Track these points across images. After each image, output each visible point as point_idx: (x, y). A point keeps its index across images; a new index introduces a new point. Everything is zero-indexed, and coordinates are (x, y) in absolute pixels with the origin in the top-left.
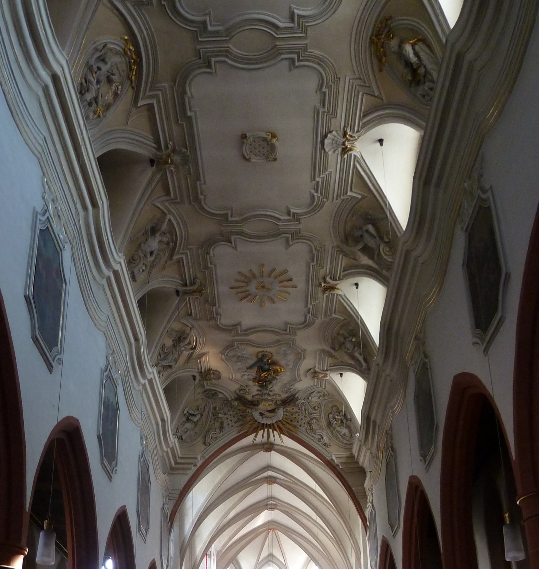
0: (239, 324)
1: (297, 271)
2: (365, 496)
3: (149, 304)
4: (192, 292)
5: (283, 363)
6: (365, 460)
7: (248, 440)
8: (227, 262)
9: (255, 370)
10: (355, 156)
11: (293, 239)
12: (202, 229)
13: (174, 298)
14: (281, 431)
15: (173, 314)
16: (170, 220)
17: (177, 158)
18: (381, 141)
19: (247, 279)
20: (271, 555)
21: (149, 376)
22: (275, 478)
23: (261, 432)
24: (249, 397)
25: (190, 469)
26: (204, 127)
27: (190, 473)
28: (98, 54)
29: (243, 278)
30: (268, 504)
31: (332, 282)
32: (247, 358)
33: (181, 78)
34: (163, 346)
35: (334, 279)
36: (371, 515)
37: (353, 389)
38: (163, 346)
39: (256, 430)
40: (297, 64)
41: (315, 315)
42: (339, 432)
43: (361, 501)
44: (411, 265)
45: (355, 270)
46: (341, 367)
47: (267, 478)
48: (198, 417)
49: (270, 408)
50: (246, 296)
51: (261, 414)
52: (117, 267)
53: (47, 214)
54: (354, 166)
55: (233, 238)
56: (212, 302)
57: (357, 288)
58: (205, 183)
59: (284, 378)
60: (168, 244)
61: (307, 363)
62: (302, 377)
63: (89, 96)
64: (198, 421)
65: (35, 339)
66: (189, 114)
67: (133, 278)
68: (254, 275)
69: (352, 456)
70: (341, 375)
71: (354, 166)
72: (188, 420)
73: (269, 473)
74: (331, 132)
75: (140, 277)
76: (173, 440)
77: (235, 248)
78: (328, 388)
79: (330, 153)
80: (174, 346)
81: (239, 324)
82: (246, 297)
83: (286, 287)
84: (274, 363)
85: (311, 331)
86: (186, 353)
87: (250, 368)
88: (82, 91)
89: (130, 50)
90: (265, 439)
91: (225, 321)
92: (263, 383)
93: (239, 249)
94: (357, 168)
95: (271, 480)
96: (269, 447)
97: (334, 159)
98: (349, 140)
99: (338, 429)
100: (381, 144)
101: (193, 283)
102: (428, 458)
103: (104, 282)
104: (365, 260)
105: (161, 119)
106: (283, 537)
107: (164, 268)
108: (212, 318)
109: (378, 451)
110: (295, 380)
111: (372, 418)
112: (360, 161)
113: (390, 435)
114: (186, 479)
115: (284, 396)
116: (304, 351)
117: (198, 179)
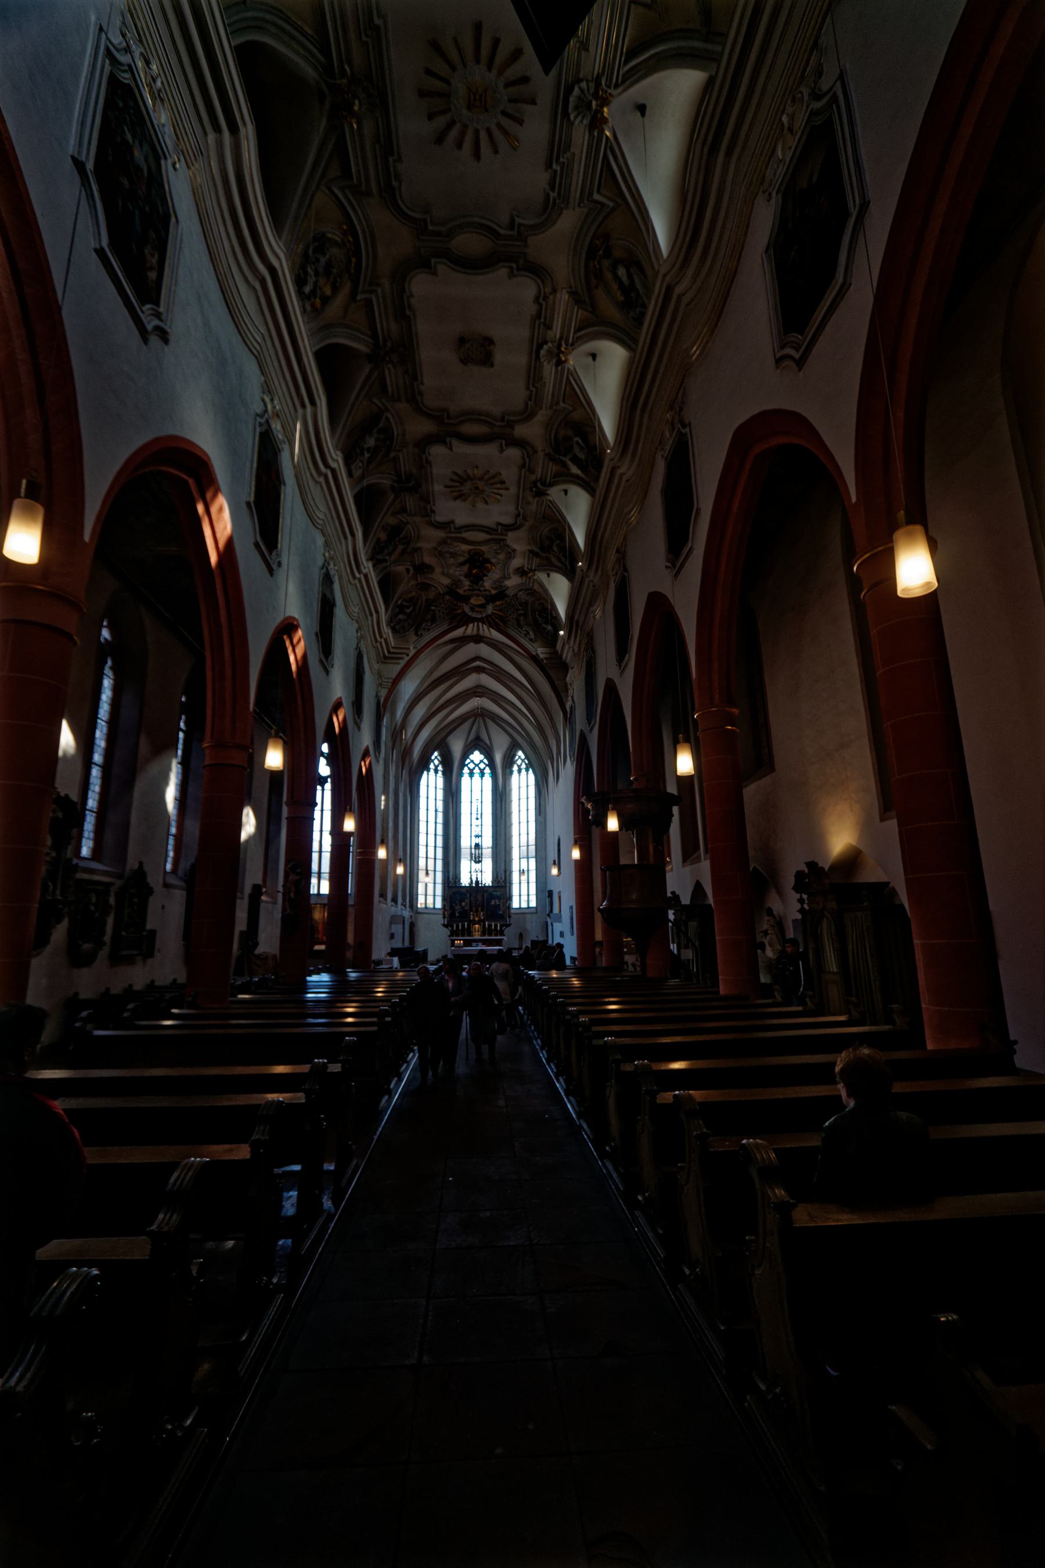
0: (453, 522)
1: (510, 474)
2: (567, 690)
3: (368, 502)
5: (493, 561)
6: (567, 655)
7: (459, 632)
8: (443, 460)
11: (507, 445)
12: (419, 427)
13: (386, 502)
14: (490, 626)
15: (388, 509)
16: (387, 418)
18: (594, 356)
19: (462, 479)
20: (478, 738)
21: (365, 571)
22: (484, 668)
23: (471, 625)
24: (461, 592)
25: (402, 658)
26: (423, 327)
27: (402, 663)
29: (455, 478)
30: (479, 691)
33: (401, 274)
34: (379, 539)
36: (571, 708)
37: (559, 591)
39: (466, 624)
41: (525, 519)
43: (563, 695)
44: (616, 481)
45: (564, 477)
46: (549, 567)
47: (475, 667)
49: (479, 603)
50: (460, 497)
51: (472, 609)
52: (334, 465)
53: (266, 416)
54: (568, 378)
56: (427, 499)
57: (643, 114)
58: (422, 383)
59: (495, 575)
61: (517, 562)
63: (307, 289)
65: (257, 545)
66: (408, 313)
67: (350, 474)
69: (557, 652)
70: (548, 575)
71: (568, 378)
72: (401, 612)
73: (478, 663)
74: (546, 343)
75: (357, 473)
76: (387, 630)
77: (451, 449)
78: (536, 587)
79: (545, 364)
81: (453, 522)
83: (499, 489)
84: (488, 561)
85: (522, 533)
86: (400, 547)
87: (462, 564)
88: (300, 282)
89: (349, 242)
90: (475, 632)
91: (440, 518)
92: (476, 580)
93: (454, 448)
94: (570, 383)
95: (479, 670)
96: (478, 639)
97: (548, 370)
98: (563, 352)
102: (623, 664)
103: (322, 480)
104: (575, 470)
105: (380, 315)
106: (490, 723)
109: (579, 647)
111: (576, 618)
112: (573, 373)
113: (590, 637)
114: (397, 668)
115: (493, 592)
116: (514, 550)
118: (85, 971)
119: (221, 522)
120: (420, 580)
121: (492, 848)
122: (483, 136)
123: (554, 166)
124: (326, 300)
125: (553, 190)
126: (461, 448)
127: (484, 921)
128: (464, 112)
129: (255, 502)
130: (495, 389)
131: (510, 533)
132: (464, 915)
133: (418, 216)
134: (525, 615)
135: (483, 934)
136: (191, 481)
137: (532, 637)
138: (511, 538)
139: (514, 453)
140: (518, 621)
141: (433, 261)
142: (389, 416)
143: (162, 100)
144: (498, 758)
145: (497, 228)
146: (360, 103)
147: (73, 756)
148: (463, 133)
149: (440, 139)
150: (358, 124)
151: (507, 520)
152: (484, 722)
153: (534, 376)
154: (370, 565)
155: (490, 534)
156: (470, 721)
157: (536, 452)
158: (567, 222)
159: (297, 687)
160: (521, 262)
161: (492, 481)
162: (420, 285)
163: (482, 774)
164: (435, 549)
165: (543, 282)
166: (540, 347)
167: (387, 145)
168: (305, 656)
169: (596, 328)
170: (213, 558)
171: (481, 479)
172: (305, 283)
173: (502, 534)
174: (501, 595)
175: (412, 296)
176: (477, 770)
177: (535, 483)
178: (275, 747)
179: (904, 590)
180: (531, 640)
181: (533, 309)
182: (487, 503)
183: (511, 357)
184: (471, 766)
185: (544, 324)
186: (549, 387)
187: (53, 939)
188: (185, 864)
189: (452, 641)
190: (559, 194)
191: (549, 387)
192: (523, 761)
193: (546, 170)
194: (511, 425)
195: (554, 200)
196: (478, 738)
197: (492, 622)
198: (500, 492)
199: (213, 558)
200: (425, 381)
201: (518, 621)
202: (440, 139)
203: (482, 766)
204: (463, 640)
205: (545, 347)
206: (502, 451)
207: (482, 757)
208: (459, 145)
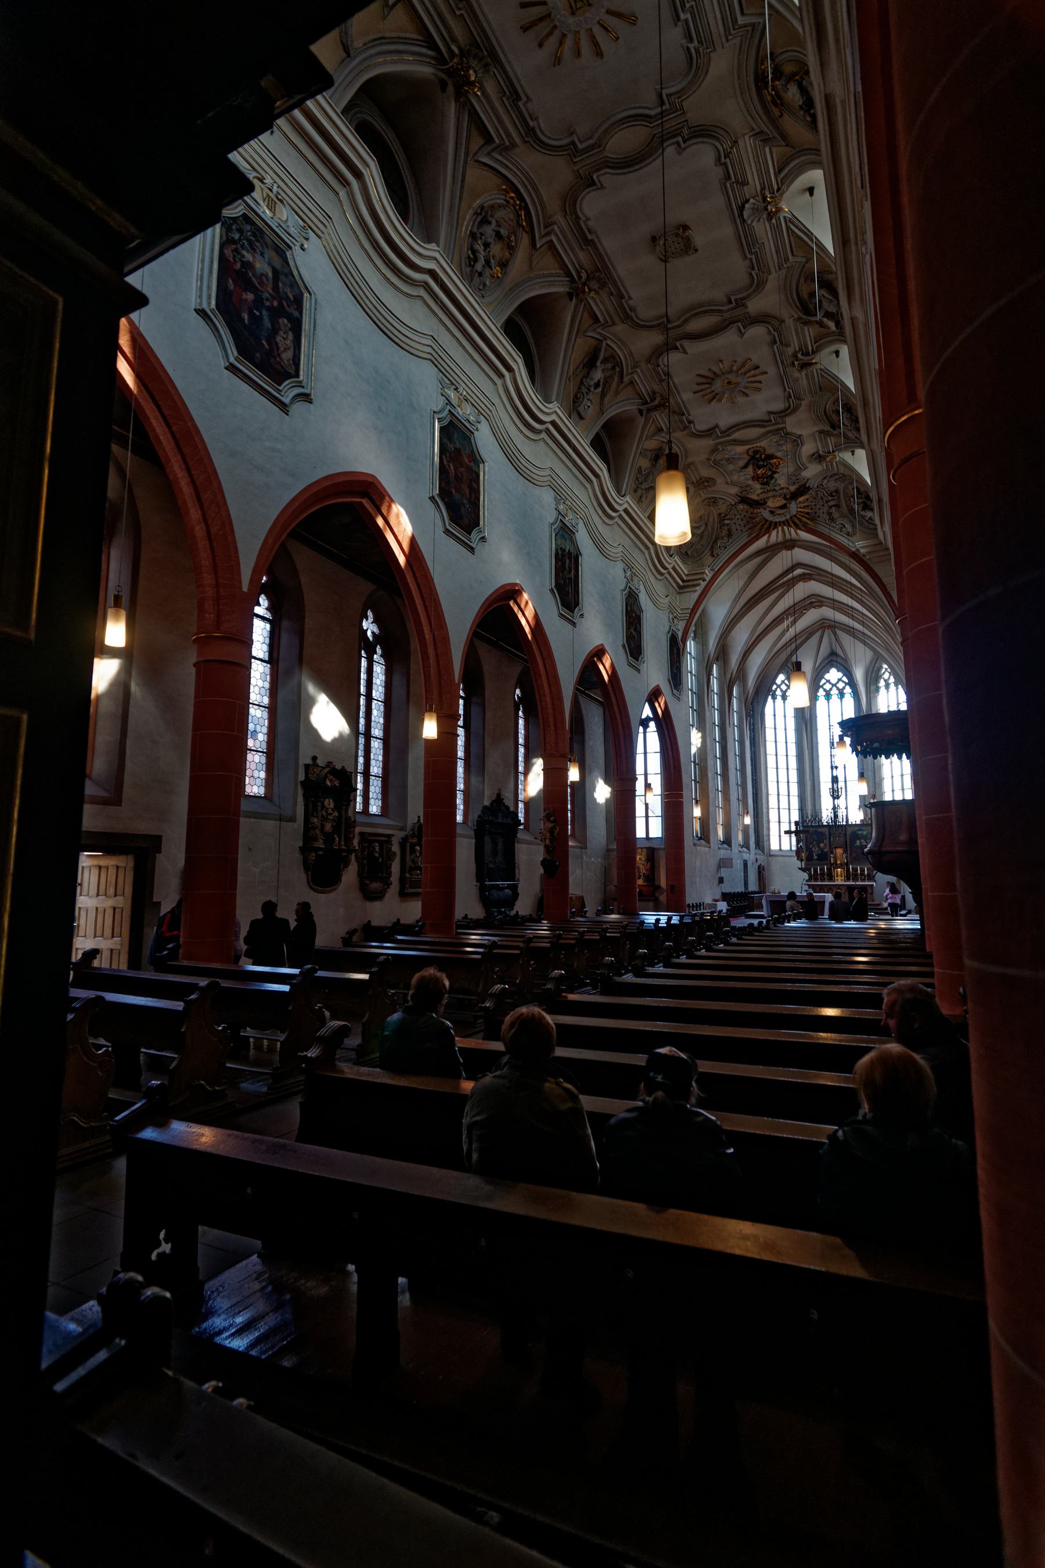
0: (717, 426)
1: (762, 356)
4: (655, 408)
5: (779, 454)
9: (750, 469)
10: (785, 218)
12: (646, 342)
14: (797, 527)
17: (594, 285)
19: (709, 379)
20: (833, 653)
23: (774, 533)
24: (754, 497)
25: (698, 585)
26: (610, 244)
27: (699, 589)
28: (479, 218)
30: (815, 601)
31: (806, 359)
32: (738, 459)
33: (570, 202)
34: (640, 470)
35: (807, 354)
38: (640, 470)
39: (768, 531)
40: (683, 146)
41: (799, 398)
42: (863, 517)
48: (702, 528)
50: (715, 397)
51: (772, 512)
54: (788, 228)
55: (678, 344)
58: (630, 298)
60: (613, 368)
61: (808, 448)
62: (807, 465)
64: (703, 532)
68: (715, 373)
73: (798, 571)
74: (747, 201)
77: (685, 352)
78: (842, 470)
80: (653, 466)
81: (717, 426)
82: (714, 398)
83: (754, 376)
84: (771, 457)
85: (802, 414)
87: (745, 467)
89: (512, 198)
90: (780, 539)
91: (701, 427)
92: (766, 480)
94: (793, 231)
96: (790, 544)
97: (761, 229)
99: (863, 513)
100: (811, 194)
101: (653, 400)
106: (840, 633)
107: (617, 393)
108: (685, 428)
110: (800, 468)
112: (793, 221)
114: (695, 596)
115: (793, 488)
116: (800, 436)
117: (622, 297)
118: (377, 904)
119: (400, 526)
120: (704, 496)
121: (635, 796)
122: (597, 30)
123: (682, 16)
124: (504, 265)
125: (691, 41)
126: (695, 348)
127: (847, 865)
128: (571, 20)
129: (440, 495)
130: (705, 277)
131: (788, 420)
132: (823, 857)
133: (565, 142)
134: (837, 506)
135: (848, 879)
136: (364, 501)
137: (850, 530)
138: (791, 424)
139: (758, 331)
140: (830, 514)
141: (595, 177)
142: (609, 342)
143: (281, 201)
144: (859, 674)
145: (647, 112)
146: (475, 71)
147: (349, 735)
148: (577, 42)
149: (557, 60)
150: (480, 89)
151: (779, 406)
152: (835, 634)
153: (747, 243)
154: (628, 498)
155: (764, 426)
156: (818, 634)
157: (783, 321)
158: (721, 64)
159: (534, 647)
160: (685, 131)
161: (743, 370)
162: (591, 205)
163: (842, 694)
164: (708, 459)
165: (718, 139)
166: (741, 209)
167: (513, 95)
168: (536, 616)
169: (797, 161)
170: (402, 559)
171: (731, 371)
172: (476, 260)
173: (777, 423)
174: (803, 490)
175: (588, 219)
176: (835, 691)
177: (795, 356)
178: (431, 718)
179: (660, 536)
180: (848, 534)
181: (719, 171)
182: (747, 395)
183: (713, 232)
184: (828, 687)
185: (737, 182)
186: (770, 247)
187: (344, 878)
188: (474, 816)
189: (758, 553)
190: (700, 42)
191: (770, 247)
192: (779, 686)
193: (676, 25)
194: (741, 303)
195: (697, 51)
196: (833, 653)
197: (795, 522)
198: (758, 378)
199: (402, 559)
200: (633, 295)
201: (830, 514)
202: (557, 60)
203: (841, 685)
204: (772, 550)
205: (747, 206)
206: (742, 334)
207: (840, 675)
208: (578, 54)
